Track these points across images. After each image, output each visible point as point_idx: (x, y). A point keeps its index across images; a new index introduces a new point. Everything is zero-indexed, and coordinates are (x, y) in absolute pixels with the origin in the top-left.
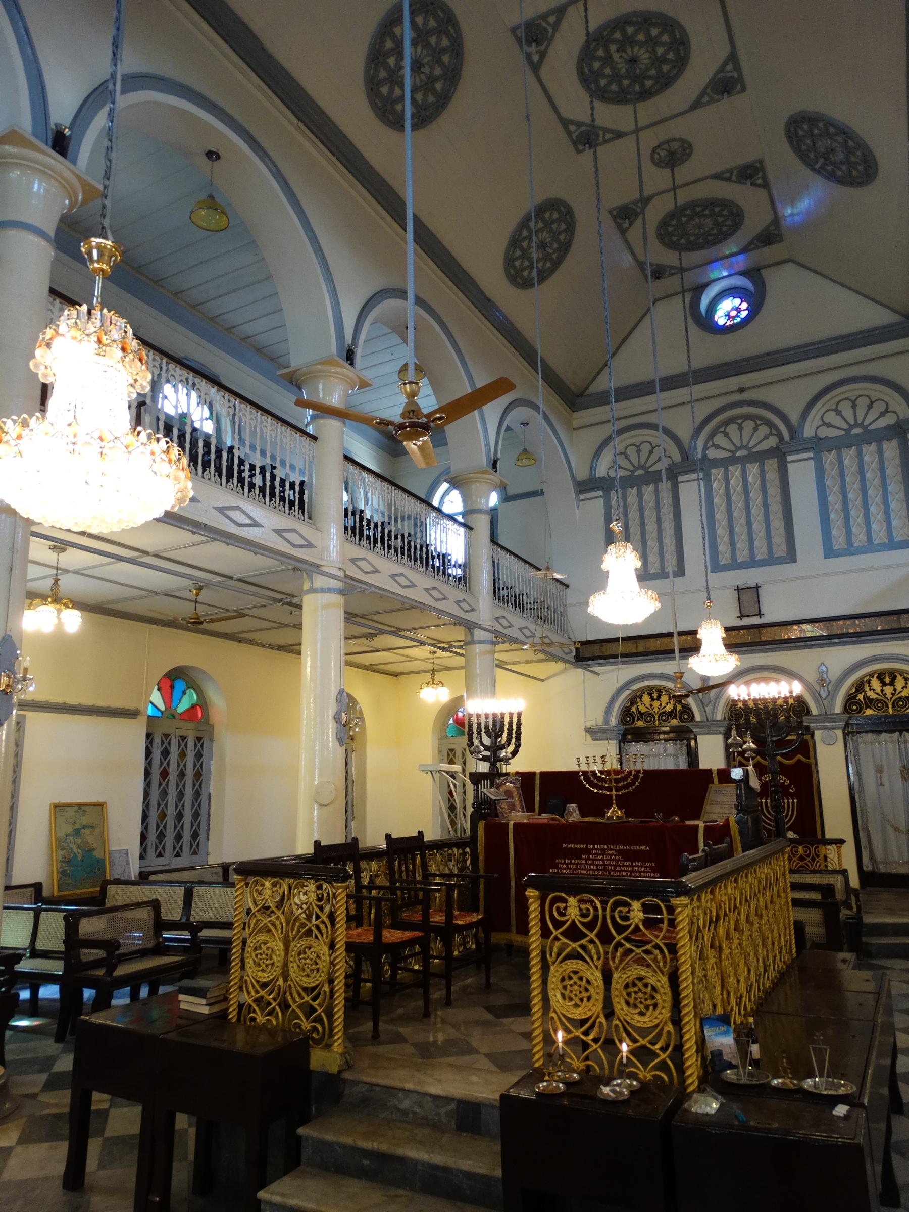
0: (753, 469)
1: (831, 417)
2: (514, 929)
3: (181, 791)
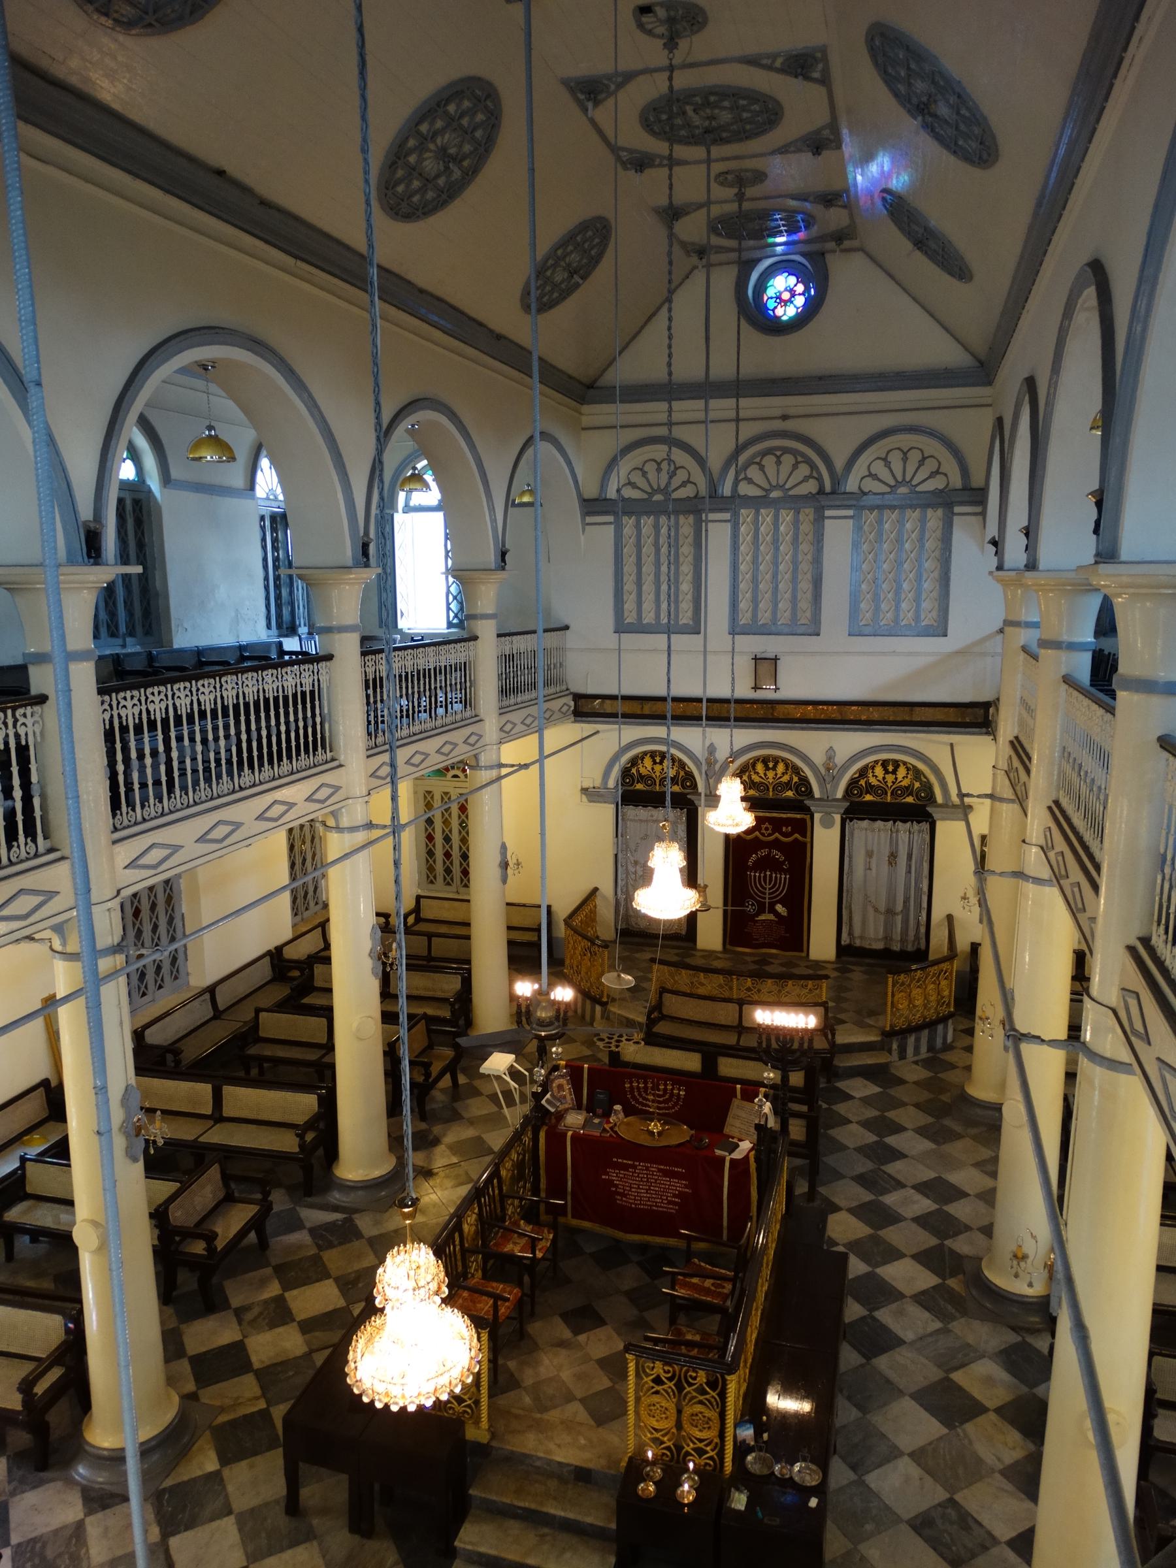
0: (786, 516)
1: (879, 468)
2: (570, 1215)
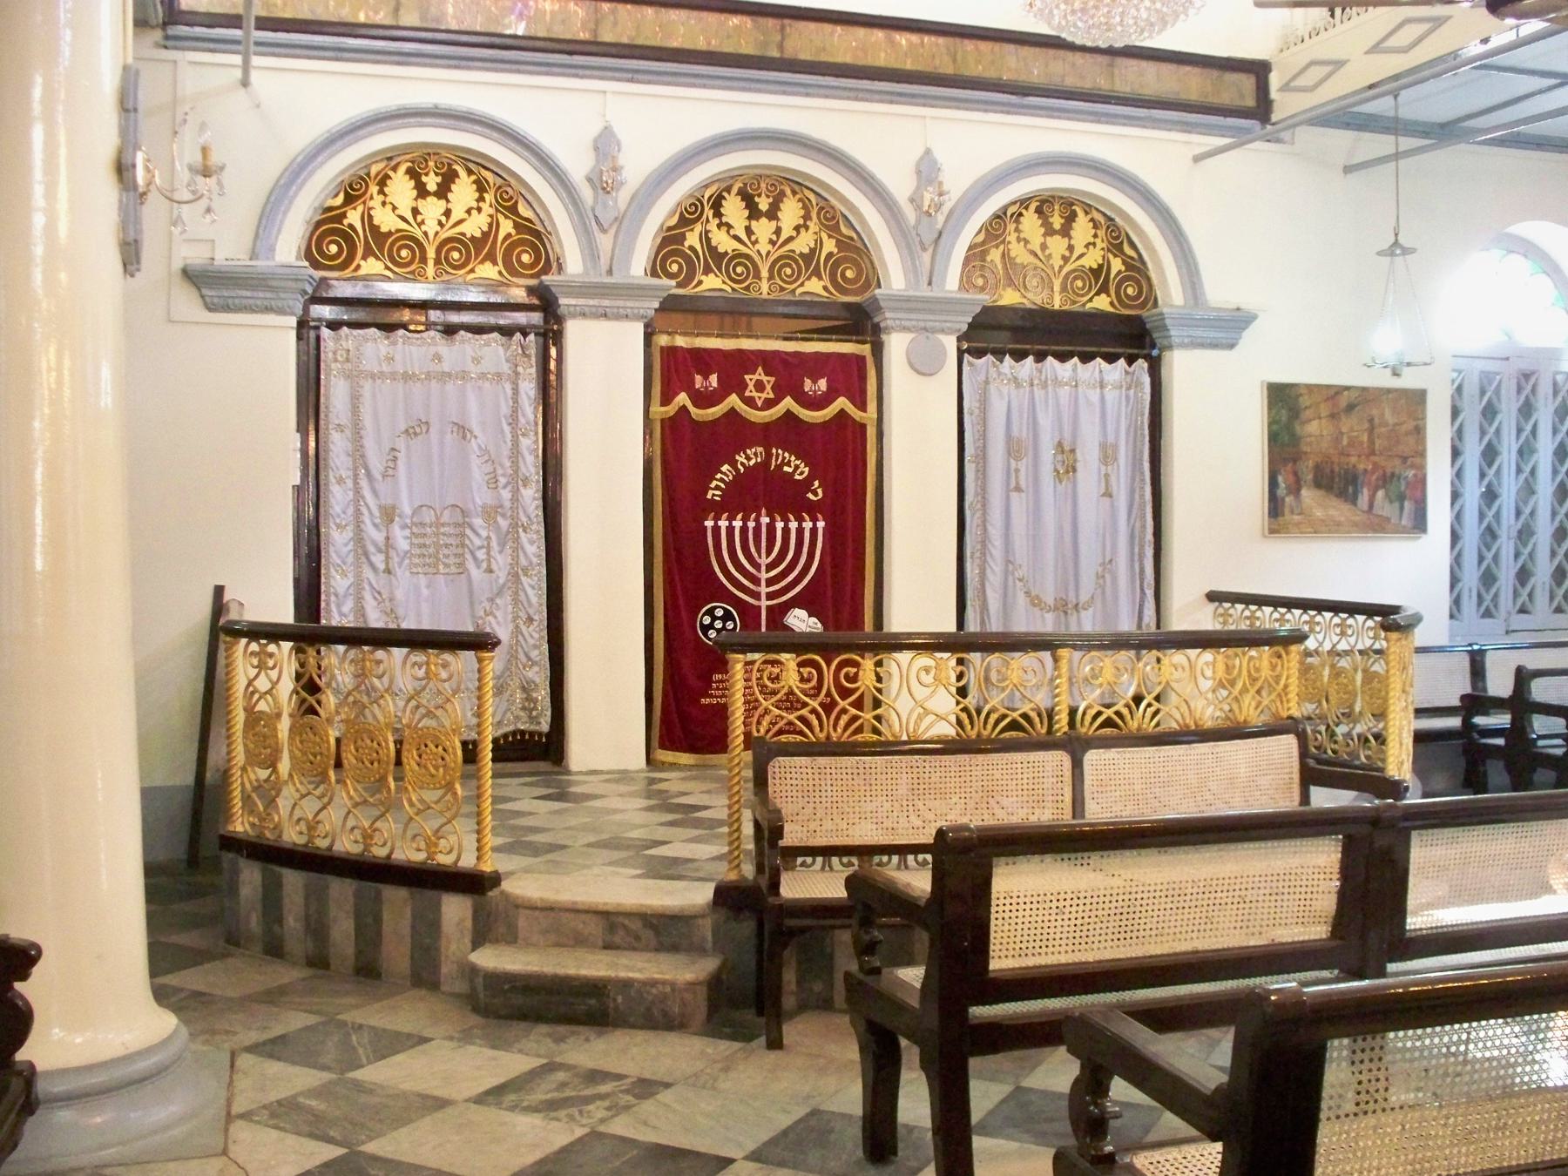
3: (1490, 465)
